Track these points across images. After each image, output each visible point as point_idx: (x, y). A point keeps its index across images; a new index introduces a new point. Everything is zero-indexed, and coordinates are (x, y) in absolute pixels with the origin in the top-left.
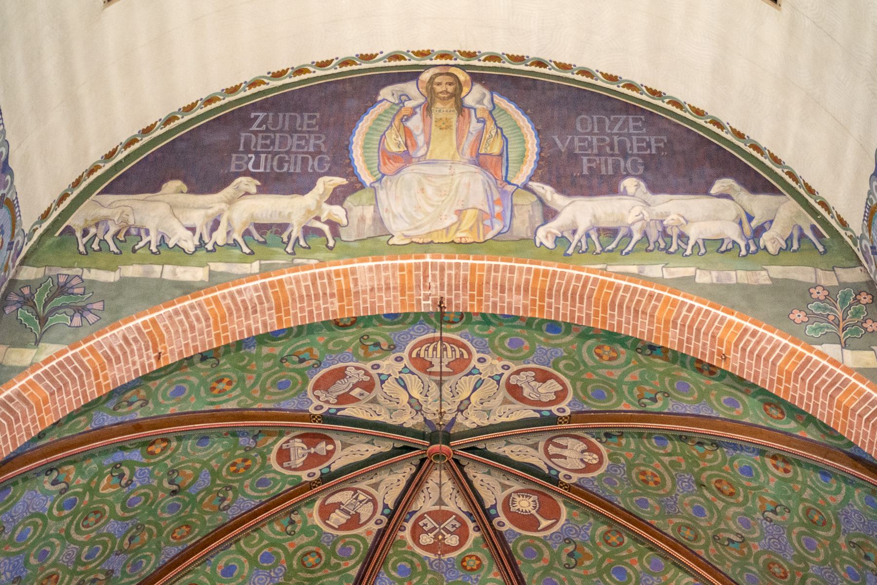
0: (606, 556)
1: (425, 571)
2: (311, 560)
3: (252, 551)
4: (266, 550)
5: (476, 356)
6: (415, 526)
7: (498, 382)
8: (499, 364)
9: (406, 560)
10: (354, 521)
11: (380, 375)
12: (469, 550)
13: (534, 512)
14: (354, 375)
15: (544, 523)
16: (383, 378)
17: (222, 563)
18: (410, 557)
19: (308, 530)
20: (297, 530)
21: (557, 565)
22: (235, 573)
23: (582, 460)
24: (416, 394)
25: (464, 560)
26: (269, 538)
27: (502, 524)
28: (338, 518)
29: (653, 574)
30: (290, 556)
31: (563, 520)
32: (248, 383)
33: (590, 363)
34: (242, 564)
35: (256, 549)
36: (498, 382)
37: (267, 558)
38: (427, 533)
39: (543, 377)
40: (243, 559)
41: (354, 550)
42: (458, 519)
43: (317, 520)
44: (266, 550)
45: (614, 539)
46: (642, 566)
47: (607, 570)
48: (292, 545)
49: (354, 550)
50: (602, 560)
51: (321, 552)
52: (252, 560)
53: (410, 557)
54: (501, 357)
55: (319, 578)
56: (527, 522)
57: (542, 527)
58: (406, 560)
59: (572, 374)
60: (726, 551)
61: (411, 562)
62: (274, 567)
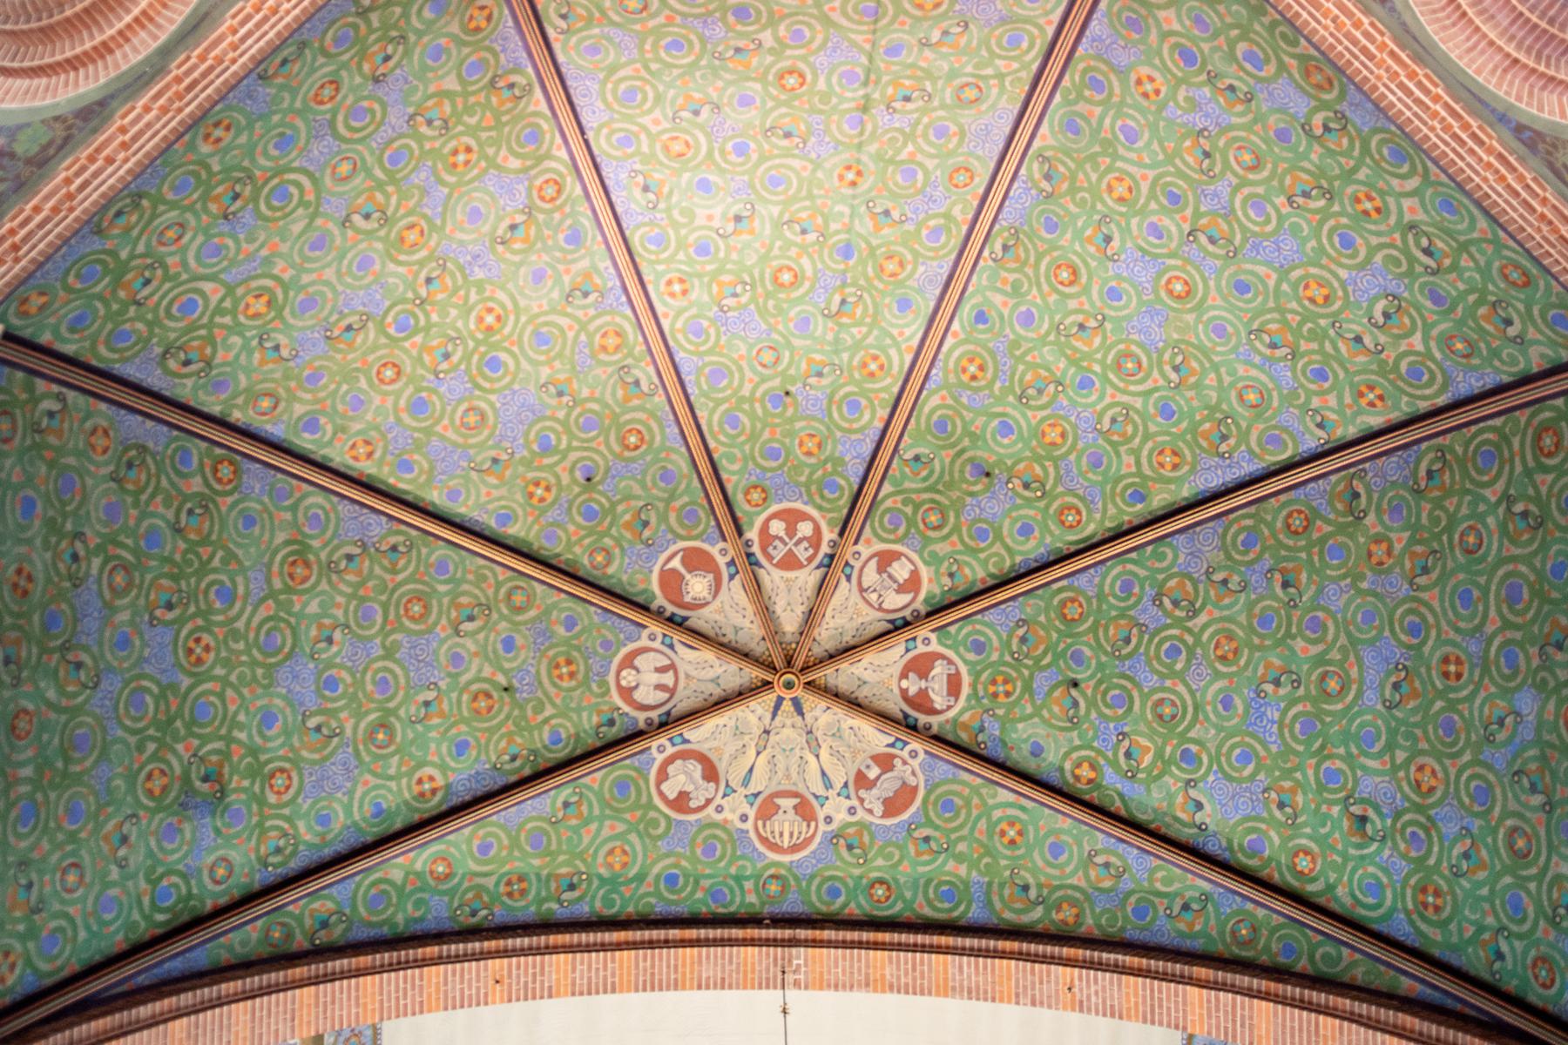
0: (606, 533)
1: (807, 485)
2: (933, 518)
3: (997, 548)
4: (983, 545)
5: (749, 825)
6: (817, 547)
7: (727, 785)
8: (727, 814)
9: (828, 500)
10: (885, 560)
11: (848, 797)
12: (759, 514)
13: (688, 577)
14: (874, 799)
15: (676, 563)
16: (845, 792)
17: (1032, 543)
18: (825, 504)
19: (934, 560)
20: (946, 564)
21: (661, 505)
22: (1019, 525)
23: (638, 671)
24: (811, 759)
25: (765, 500)
26: (978, 559)
27: (723, 552)
28: (901, 571)
29: (552, 524)
30: (956, 529)
31: (656, 569)
32: (982, 824)
33: (633, 837)
34: (1010, 535)
35: (994, 550)
36: (727, 785)
37: (982, 535)
38: (805, 538)
39: (681, 802)
40: (1008, 541)
41: (886, 520)
42: (770, 558)
43: (925, 573)
44: (983, 545)
45: (599, 558)
46: (566, 531)
47: (606, 512)
48: (953, 544)
49: (886, 520)
50: (612, 524)
51: (922, 526)
52: (999, 537)
53: (825, 504)
54: (723, 825)
55: (926, 490)
56: (697, 561)
57: (678, 558)
58: (828, 500)
59: (652, 814)
60: (476, 597)
61: (823, 497)
62: (975, 521)
